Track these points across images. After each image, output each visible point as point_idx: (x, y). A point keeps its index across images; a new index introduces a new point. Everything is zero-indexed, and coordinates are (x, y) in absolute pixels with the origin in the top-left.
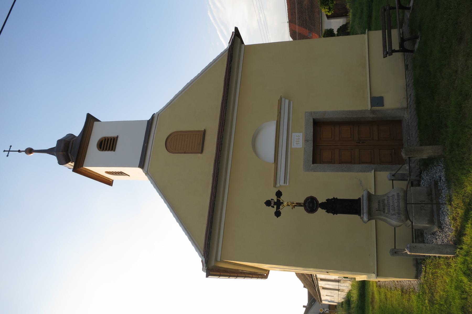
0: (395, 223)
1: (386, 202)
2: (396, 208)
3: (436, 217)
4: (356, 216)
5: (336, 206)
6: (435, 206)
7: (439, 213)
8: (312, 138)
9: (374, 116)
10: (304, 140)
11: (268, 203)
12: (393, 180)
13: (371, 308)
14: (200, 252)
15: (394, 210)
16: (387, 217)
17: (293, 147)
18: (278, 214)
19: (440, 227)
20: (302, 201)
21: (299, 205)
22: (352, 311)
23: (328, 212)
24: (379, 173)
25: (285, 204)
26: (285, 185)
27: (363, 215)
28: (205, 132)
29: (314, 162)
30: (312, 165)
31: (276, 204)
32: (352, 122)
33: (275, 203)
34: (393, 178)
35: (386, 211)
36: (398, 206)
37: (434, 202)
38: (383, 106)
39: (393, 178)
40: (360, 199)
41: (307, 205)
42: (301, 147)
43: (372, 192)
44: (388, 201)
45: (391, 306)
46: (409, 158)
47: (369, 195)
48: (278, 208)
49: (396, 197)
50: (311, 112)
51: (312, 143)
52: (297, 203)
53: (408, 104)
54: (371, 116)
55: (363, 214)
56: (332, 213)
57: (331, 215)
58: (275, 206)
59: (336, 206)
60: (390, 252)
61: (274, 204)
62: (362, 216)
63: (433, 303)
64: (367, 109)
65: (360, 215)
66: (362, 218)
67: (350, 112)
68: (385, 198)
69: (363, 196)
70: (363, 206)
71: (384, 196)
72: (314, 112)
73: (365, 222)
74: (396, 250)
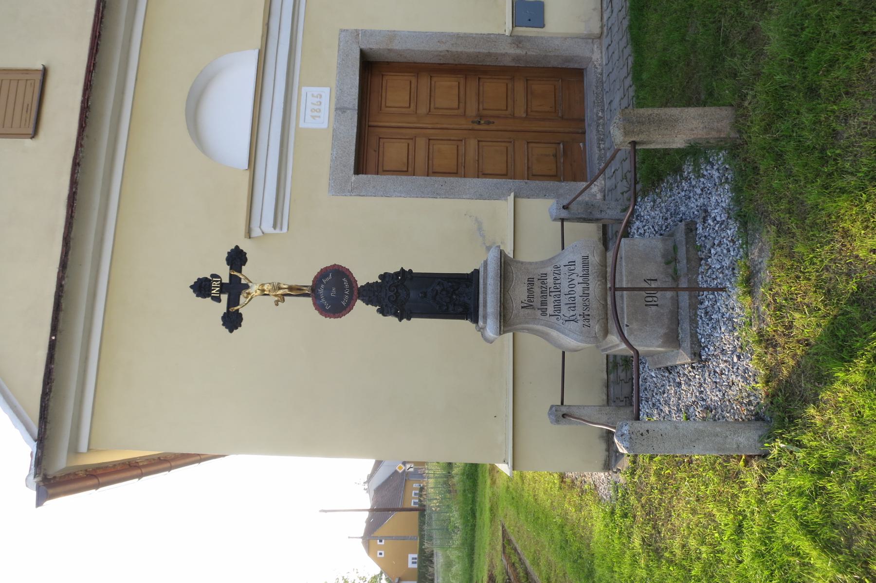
0: (570, 342)
1: (550, 281)
2: (579, 300)
3: (686, 325)
4: (465, 325)
5: (410, 295)
6: (684, 297)
7: (696, 315)
8: (356, 102)
9: (518, 51)
10: (333, 107)
11: (202, 288)
12: (562, 220)
13: (489, 482)
14: (28, 429)
15: (572, 306)
16: (551, 327)
17: (302, 125)
18: (232, 321)
19: (698, 356)
20: (307, 281)
21: (296, 291)
22: (456, 480)
23: (383, 312)
24: (524, 202)
25: (254, 289)
26: (278, 231)
27: (485, 322)
28: (45, 72)
29: (359, 169)
30: (354, 178)
31: (226, 290)
32: (463, 68)
33: (223, 288)
34: (564, 214)
35: (550, 310)
36: (585, 295)
37: (683, 284)
38: (543, 26)
39: (564, 214)
40: (477, 272)
41: (321, 291)
42: (325, 126)
43: (509, 252)
44: (555, 279)
45: (531, 499)
46: (634, 143)
47: (505, 265)
48: (233, 301)
49: (579, 269)
50: (356, 30)
51: (356, 116)
52: (291, 288)
53: (602, 27)
54: (513, 51)
55: (485, 318)
56: (395, 314)
57: (392, 320)
58: (224, 297)
59: (410, 295)
60: (550, 414)
61: (221, 292)
62: (481, 323)
63: (658, 553)
64: (502, 32)
65: (475, 320)
66: (482, 330)
67: (458, 36)
68: (549, 270)
69: (486, 264)
70: (485, 293)
71: (543, 264)
72: (364, 32)
73: (490, 342)
74: (564, 410)
